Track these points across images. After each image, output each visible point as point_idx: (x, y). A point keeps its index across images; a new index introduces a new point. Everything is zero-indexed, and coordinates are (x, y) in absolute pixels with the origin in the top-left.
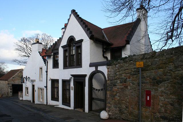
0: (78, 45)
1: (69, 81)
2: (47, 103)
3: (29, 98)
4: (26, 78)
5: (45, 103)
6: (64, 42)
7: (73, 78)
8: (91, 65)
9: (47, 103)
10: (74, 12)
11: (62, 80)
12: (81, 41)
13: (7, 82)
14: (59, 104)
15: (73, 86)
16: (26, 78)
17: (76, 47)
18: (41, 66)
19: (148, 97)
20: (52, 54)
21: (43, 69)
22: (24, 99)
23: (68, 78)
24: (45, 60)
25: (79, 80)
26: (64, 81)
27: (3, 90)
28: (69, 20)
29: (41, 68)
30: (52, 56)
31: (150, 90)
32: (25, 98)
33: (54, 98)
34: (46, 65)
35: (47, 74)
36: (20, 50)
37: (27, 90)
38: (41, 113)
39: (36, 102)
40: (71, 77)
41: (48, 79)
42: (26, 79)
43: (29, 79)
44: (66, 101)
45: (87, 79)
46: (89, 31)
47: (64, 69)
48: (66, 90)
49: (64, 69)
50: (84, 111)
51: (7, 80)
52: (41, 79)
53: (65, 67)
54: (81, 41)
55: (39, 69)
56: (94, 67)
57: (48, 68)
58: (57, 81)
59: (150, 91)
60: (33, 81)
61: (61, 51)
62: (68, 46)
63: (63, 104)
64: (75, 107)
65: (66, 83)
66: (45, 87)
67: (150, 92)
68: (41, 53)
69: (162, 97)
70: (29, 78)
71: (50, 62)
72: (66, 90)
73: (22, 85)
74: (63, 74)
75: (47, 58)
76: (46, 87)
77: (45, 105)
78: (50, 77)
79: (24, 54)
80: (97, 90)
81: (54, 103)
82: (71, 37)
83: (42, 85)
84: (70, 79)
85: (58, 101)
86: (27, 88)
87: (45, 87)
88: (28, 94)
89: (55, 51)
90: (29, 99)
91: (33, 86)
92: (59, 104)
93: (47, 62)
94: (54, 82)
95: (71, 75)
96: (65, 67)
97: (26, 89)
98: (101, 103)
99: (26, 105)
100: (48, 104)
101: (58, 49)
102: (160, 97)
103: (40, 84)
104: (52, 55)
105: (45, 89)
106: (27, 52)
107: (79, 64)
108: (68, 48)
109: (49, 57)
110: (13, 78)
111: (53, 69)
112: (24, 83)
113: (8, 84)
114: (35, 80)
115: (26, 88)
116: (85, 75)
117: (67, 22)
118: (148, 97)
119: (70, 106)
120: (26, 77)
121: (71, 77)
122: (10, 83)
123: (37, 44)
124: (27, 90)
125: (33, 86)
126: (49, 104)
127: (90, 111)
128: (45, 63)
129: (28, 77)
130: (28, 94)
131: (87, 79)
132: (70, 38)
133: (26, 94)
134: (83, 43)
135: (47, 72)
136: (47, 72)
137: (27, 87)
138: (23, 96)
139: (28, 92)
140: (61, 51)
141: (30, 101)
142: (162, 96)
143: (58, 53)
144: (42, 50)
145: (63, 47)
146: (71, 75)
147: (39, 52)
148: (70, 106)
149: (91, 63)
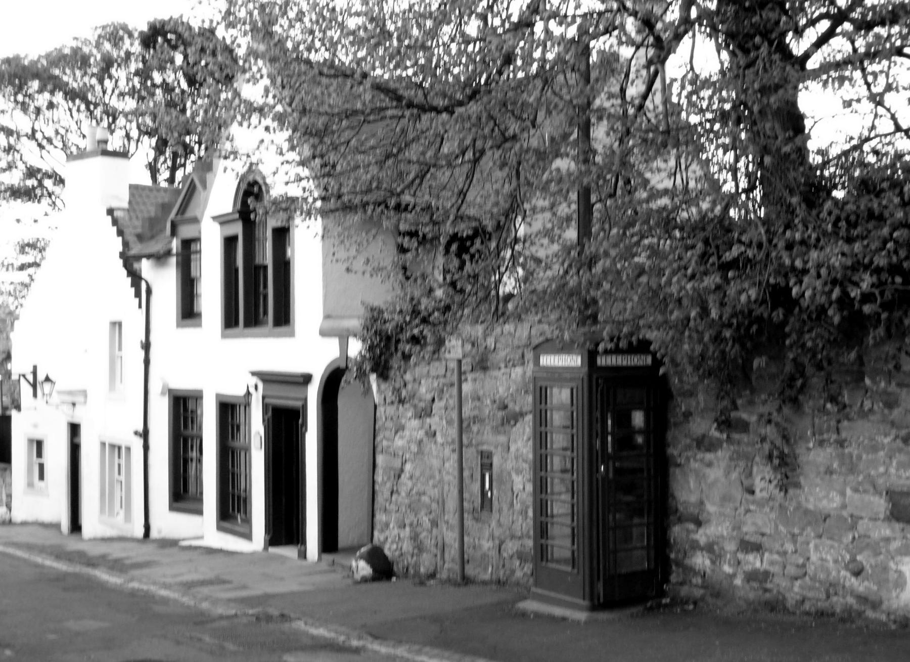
5: (140, 532)
11: (218, 396)
23: (235, 389)
24: (136, 278)
29: (117, 326)
33: (183, 494)
34: (140, 306)
35: (147, 362)
38: (103, 575)
41: (155, 388)
42: (34, 386)
43: (47, 387)
44: (232, 508)
50: (303, 555)
55: (107, 327)
66: (136, 433)
70: (47, 379)
71: (164, 281)
74: (223, 364)
76: (145, 434)
81: (170, 523)
84: (248, 393)
85: (200, 512)
87: (136, 433)
90: (47, 516)
91: (74, 429)
93: (149, 292)
95: (254, 374)
99: (41, 549)
100: (154, 534)
105: (137, 445)
112: (18, 408)
114: (84, 393)
119: (248, 536)
120: (35, 373)
121: (254, 380)
124: (39, 454)
125: (74, 429)
126: (160, 532)
128: (138, 294)
129: (41, 377)
133: (30, 485)
137: (38, 435)
138: (9, 496)
139: (41, 467)
141: (57, 526)
144: (126, 197)
145: (222, 220)
146: (254, 374)
147: (110, 212)
148: (248, 536)
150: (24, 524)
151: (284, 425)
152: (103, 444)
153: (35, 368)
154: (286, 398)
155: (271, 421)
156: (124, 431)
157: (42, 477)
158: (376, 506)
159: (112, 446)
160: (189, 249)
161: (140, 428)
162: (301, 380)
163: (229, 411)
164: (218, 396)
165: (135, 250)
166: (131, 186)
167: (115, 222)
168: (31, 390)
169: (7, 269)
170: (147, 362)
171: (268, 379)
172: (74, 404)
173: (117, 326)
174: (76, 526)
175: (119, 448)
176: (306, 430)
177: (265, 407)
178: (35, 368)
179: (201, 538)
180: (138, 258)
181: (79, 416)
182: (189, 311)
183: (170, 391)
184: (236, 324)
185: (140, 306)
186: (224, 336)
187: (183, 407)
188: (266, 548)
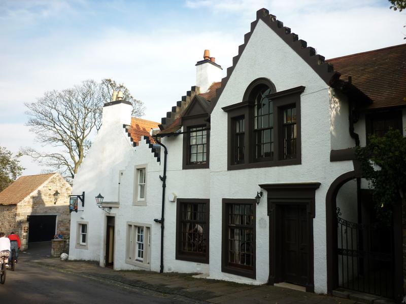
1: (249, 205)
2: (162, 267)
3: (94, 251)
4: (81, 197)
5: (158, 269)
6: (234, 95)
7: (265, 194)
8: (336, 156)
9: (162, 267)
10: (263, 15)
14: (214, 269)
15: (267, 218)
16: (81, 197)
17: (186, 127)
18: (140, 163)
20: (182, 130)
22: (72, 256)
25: (290, 204)
26: (229, 205)
29: (141, 171)
30: (182, 136)
32: (74, 254)
35: (164, 186)
36: (43, 125)
37: (83, 231)
39: (120, 263)
40: (259, 189)
41: (169, 197)
45: (320, 199)
47: (229, 169)
49: (229, 169)
50: (308, 281)
52: (139, 199)
53: (236, 160)
56: (353, 170)
57: (167, 169)
58: (205, 203)
61: (219, 122)
63: (224, 270)
64: (278, 270)
65: (238, 212)
66: (156, 221)
68: (127, 127)
74: (222, 183)
75: (165, 140)
76: (161, 222)
77: (155, 273)
79: (51, 134)
83: (148, 215)
84: (258, 197)
92: (214, 269)
93: (166, 153)
94: (192, 212)
95: (260, 185)
96: (236, 160)
97: (79, 231)
100: (166, 270)
104: (180, 133)
105: (156, 229)
106: (60, 128)
107: (290, 153)
111: (184, 170)
112: (76, 211)
115: (80, 224)
116: (316, 186)
127: (334, 289)
131: (320, 199)
132: (259, 83)
134: (304, 98)
135: (163, 179)
137: (84, 222)
140: (219, 122)
141: (97, 263)
146: (261, 186)
148: (253, 276)
149: (333, 152)
150: (76, 261)
153: (84, 193)
157: (84, 241)
159: (136, 226)
162: (110, 261)
167: (127, 131)
168: (81, 203)
170: (164, 186)
173: (141, 171)
174: (109, 264)
178: (84, 193)
179: (209, 276)
181: (113, 212)
185: (159, 160)
186: (88, 222)
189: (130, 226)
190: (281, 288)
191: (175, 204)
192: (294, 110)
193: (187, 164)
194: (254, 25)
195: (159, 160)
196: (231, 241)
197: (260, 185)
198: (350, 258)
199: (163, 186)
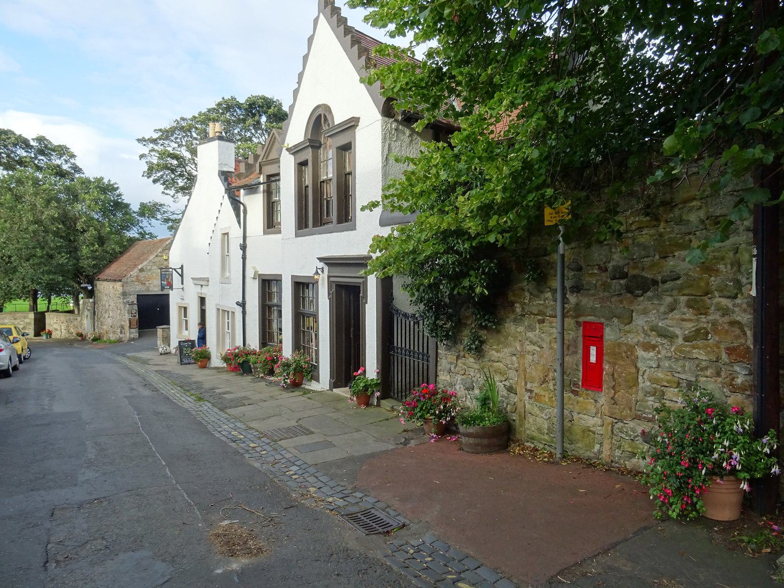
0: (342, 140)
4: (179, 271)
11: (292, 276)
12: (352, 124)
13: (118, 285)
16: (179, 271)
19: (593, 350)
21: (230, 236)
23: (308, 268)
24: (236, 204)
27: (107, 315)
28: (296, 92)
31: (602, 320)
35: (244, 258)
41: (250, 274)
46: (349, 37)
47: (297, 236)
48: (303, 318)
51: (120, 281)
54: (352, 124)
59: (602, 324)
60: (203, 282)
62: (312, 147)
66: (238, 303)
67: (600, 327)
69: (651, 354)
71: (255, 204)
72: (303, 318)
73: (167, 296)
74: (297, 255)
75: (246, 194)
76: (243, 305)
78: (254, 268)
80: (406, 315)
82: (320, 111)
86: (185, 309)
87: (238, 303)
88: (187, 329)
89: (269, 170)
91: (202, 300)
94: (268, 285)
95: (318, 258)
98: (421, 348)
101: (277, 161)
102: (640, 353)
103: (223, 296)
104: (260, 183)
105: (238, 310)
108: (308, 155)
109: (251, 189)
110: (142, 270)
113: (124, 294)
115: (180, 307)
117: (292, 102)
118: (593, 350)
121: (321, 265)
122: (129, 289)
123: (217, 142)
124: (185, 316)
125: (202, 300)
130: (187, 329)
135: (244, 247)
136: (244, 247)
139: (186, 321)
142: (649, 347)
143: (278, 174)
145: (295, 151)
146: (735, 207)
151: (348, 299)
152: (218, 309)
154: (348, 276)
155: (334, 293)
156: (231, 303)
158: (439, 368)
159: (224, 311)
160: (273, 178)
161: (240, 300)
163: (301, 286)
164: (292, 276)
165: (237, 183)
166: (359, 118)
169: (387, 3)
170: (244, 258)
171: (331, 262)
172: (202, 286)
175: (228, 312)
176: (366, 303)
177: (330, 284)
180: (238, 188)
181: (205, 292)
182: (271, 223)
183: (260, 275)
184: (306, 226)
187: (268, 285)
188: (331, 389)
189: (218, 309)
190: (339, 396)
191: (257, 281)
192: (276, 165)
193: (268, 227)
194: (316, 21)
195: (239, 222)
196: (304, 332)
197: (318, 258)
198: (412, 359)
199: (243, 258)
